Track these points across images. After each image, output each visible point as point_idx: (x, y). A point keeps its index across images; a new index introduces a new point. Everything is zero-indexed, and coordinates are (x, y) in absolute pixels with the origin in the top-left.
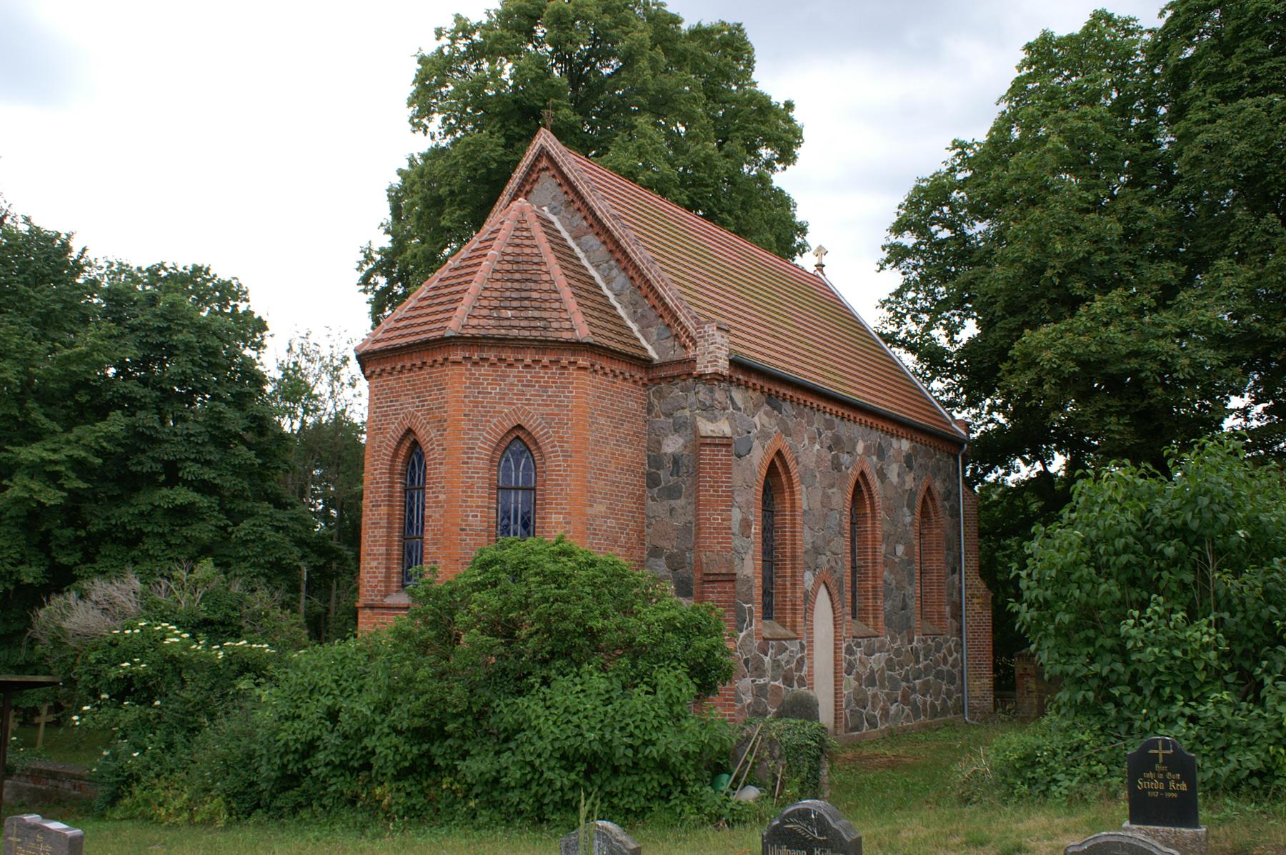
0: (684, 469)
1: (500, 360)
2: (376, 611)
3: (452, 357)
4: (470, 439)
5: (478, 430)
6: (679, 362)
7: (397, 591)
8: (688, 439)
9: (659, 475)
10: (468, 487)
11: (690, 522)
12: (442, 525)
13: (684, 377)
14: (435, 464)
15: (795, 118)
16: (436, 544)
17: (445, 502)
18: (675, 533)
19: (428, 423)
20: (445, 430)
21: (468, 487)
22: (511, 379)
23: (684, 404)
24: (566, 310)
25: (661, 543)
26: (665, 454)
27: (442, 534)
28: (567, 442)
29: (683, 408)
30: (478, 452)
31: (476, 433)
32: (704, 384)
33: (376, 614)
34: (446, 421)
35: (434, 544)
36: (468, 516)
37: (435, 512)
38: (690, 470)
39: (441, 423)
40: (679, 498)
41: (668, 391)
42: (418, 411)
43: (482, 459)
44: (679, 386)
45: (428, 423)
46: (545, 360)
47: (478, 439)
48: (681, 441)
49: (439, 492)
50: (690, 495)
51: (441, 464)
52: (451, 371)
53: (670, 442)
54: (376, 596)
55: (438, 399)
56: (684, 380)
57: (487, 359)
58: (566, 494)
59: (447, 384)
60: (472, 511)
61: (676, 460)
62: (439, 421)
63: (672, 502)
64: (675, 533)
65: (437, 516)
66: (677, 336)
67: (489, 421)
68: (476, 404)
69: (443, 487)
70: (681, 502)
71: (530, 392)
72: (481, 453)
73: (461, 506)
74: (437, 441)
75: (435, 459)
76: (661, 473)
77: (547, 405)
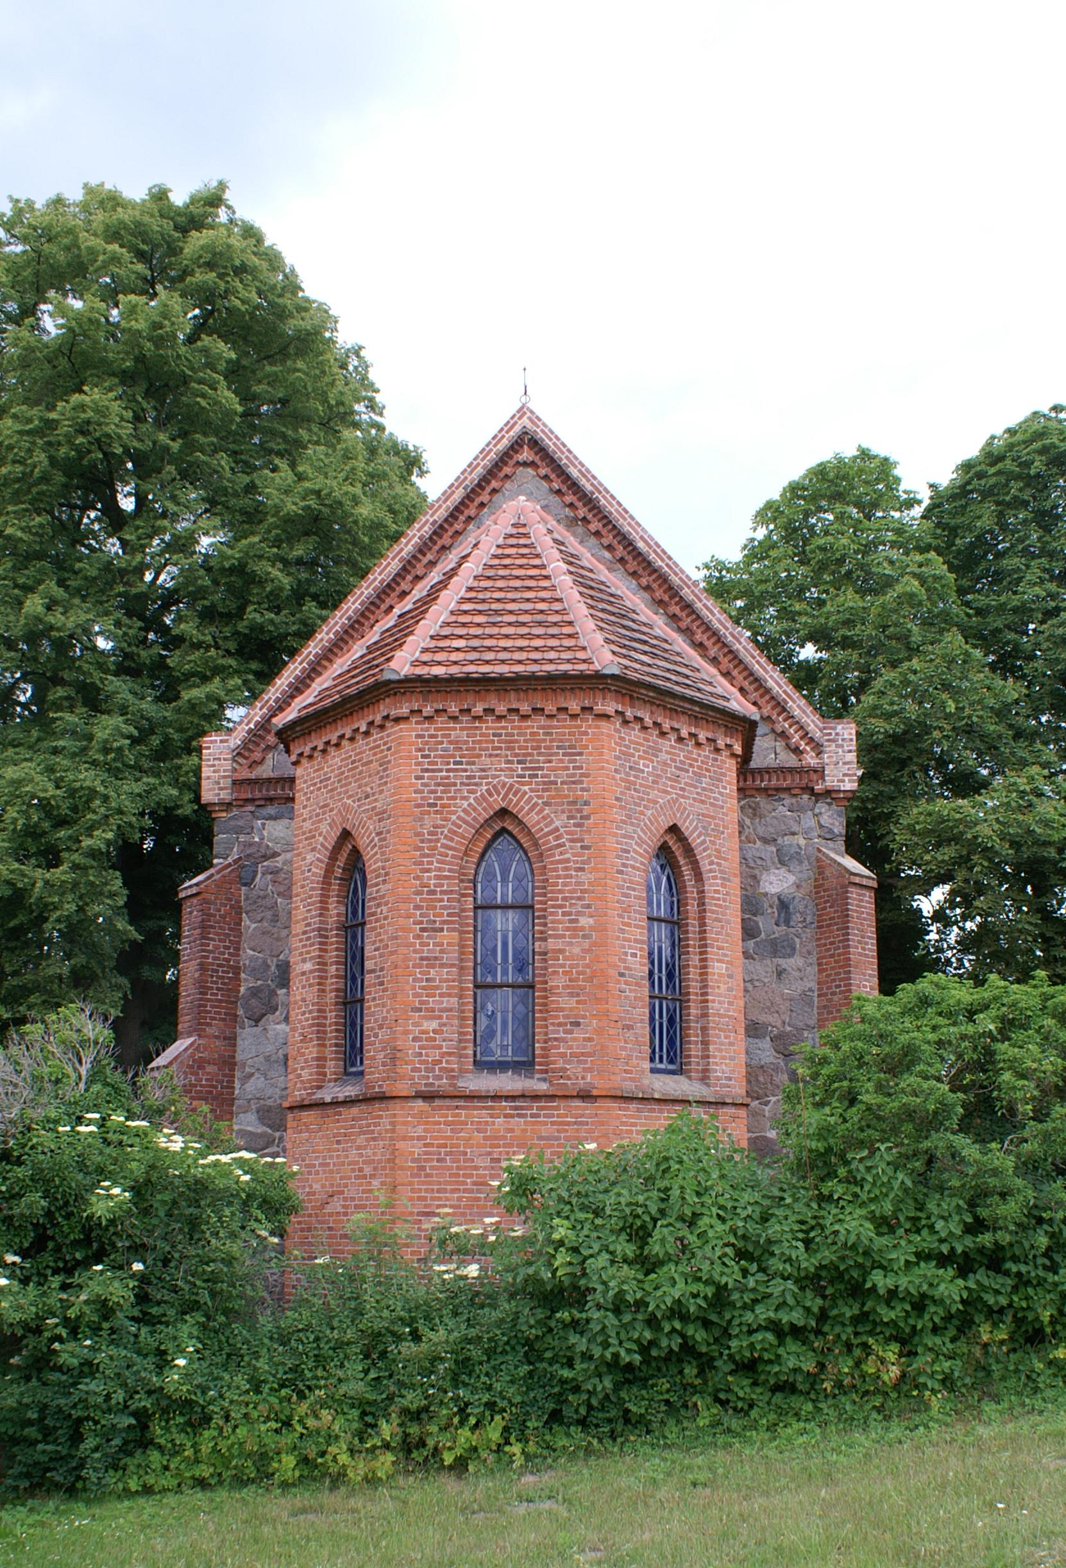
0: (797, 918)
1: (535, 710)
2: (437, 1103)
3: (599, 708)
4: (624, 836)
5: (632, 824)
6: (791, 770)
7: (336, 1080)
8: (805, 876)
9: (757, 923)
10: (624, 910)
11: (810, 990)
12: (588, 966)
13: (797, 791)
14: (566, 869)
15: (312, 297)
16: (578, 995)
17: (592, 928)
18: (787, 1004)
19: (546, 804)
20: (587, 817)
21: (624, 910)
22: (664, 756)
23: (795, 828)
24: (584, 648)
25: (763, 1018)
26: (766, 895)
27: (590, 979)
28: (726, 859)
29: (793, 834)
30: (633, 858)
31: (630, 828)
32: (829, 804)
33: (441, 1108)
34: (586, 803)
35: (571, 995)
36: (626, 954)
37: (571, 944)
38: (809, 919)
39: (578, 810)
40: (791, 956)
41: (769, 807)
42: (523, 784)
43: (638, 869)
44: (786, 802)
45: (546, 804)
46: (428, 710)
47: (632, 838)
48: (792, 879)
49: (579, 913)
50: (809, 953)
51: (582, 869)
52: (588, 724)
53: (772, 878)
54: (440, 1078)
55: (567, 768)
56: (795, 795)
57: (641, 720)
58: (727, 935)
59: (586, 747)
60: (630, 947)
61: (783, 905)
62: (574, 803)
63: (781, 961)
64: (787, 1004)
65: (576, 950)
66: (783, 735)
67: (642, 813)
68: (629, 785)
69: (589, 906)
70: (796, 961)
71: (686, 778)
72: (636, 860)
73: (618, 938)
74: (567, 833)
75: (567, 860)
76: (760, 920)
77: (702, 802)
